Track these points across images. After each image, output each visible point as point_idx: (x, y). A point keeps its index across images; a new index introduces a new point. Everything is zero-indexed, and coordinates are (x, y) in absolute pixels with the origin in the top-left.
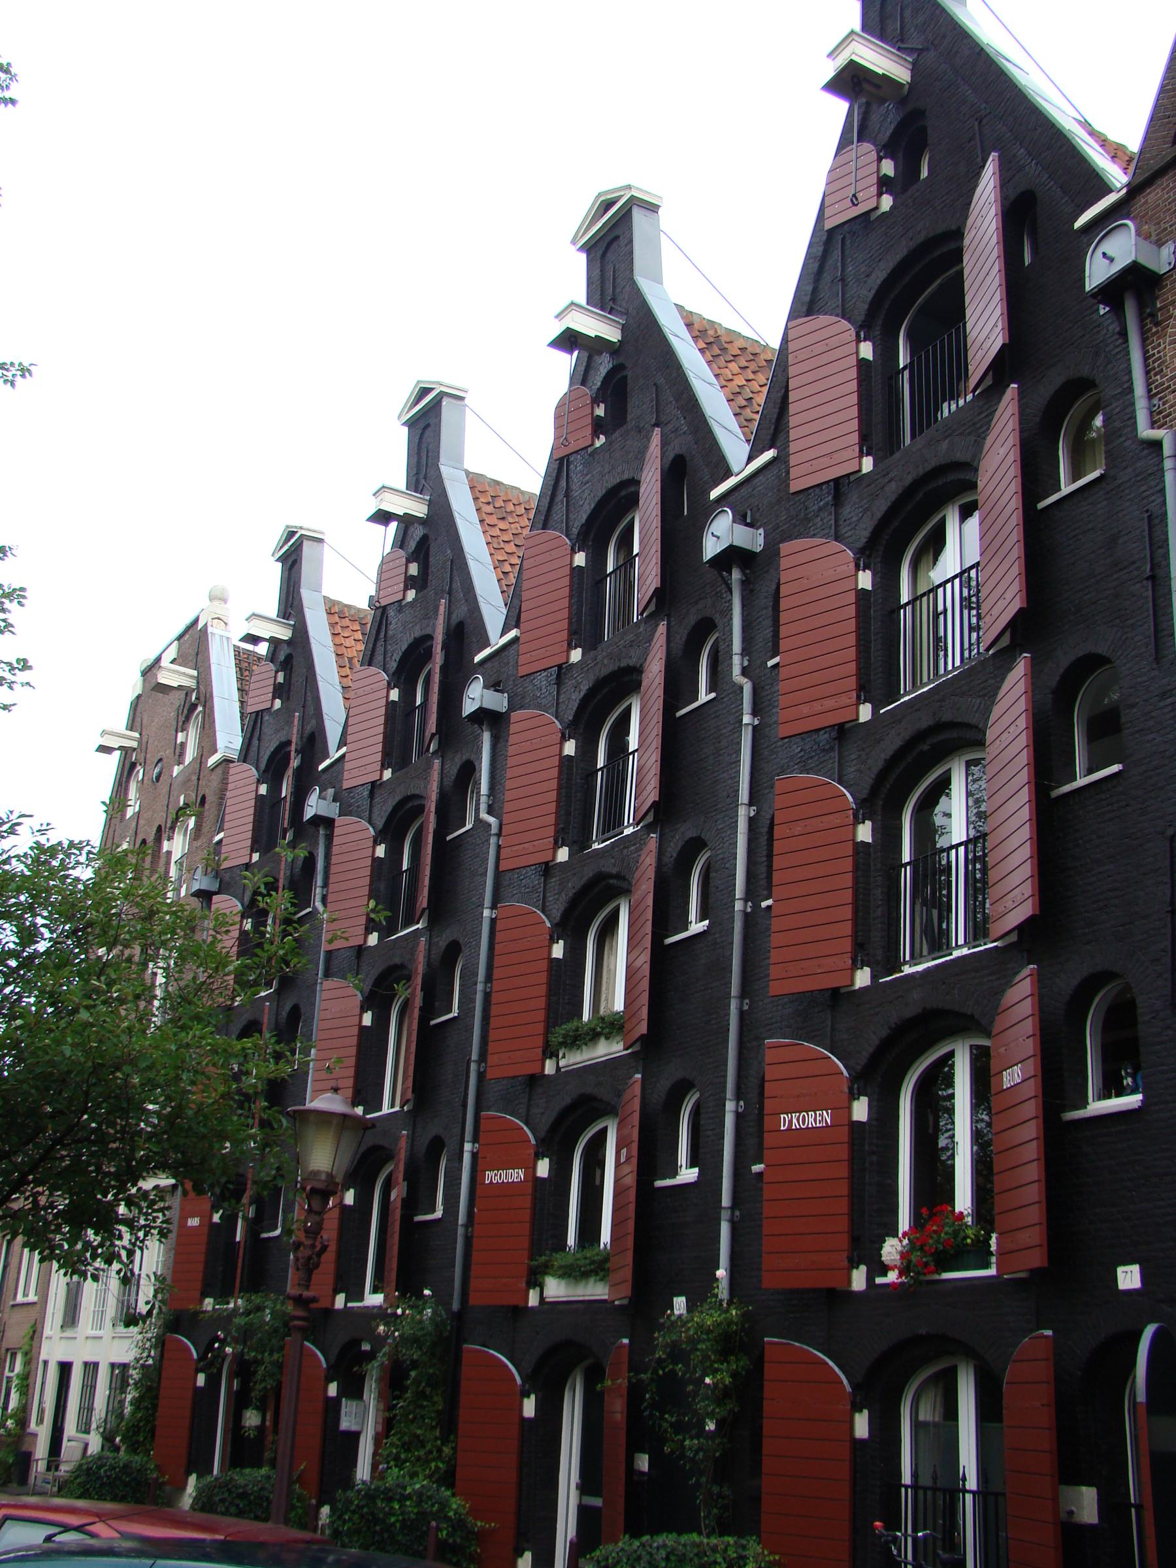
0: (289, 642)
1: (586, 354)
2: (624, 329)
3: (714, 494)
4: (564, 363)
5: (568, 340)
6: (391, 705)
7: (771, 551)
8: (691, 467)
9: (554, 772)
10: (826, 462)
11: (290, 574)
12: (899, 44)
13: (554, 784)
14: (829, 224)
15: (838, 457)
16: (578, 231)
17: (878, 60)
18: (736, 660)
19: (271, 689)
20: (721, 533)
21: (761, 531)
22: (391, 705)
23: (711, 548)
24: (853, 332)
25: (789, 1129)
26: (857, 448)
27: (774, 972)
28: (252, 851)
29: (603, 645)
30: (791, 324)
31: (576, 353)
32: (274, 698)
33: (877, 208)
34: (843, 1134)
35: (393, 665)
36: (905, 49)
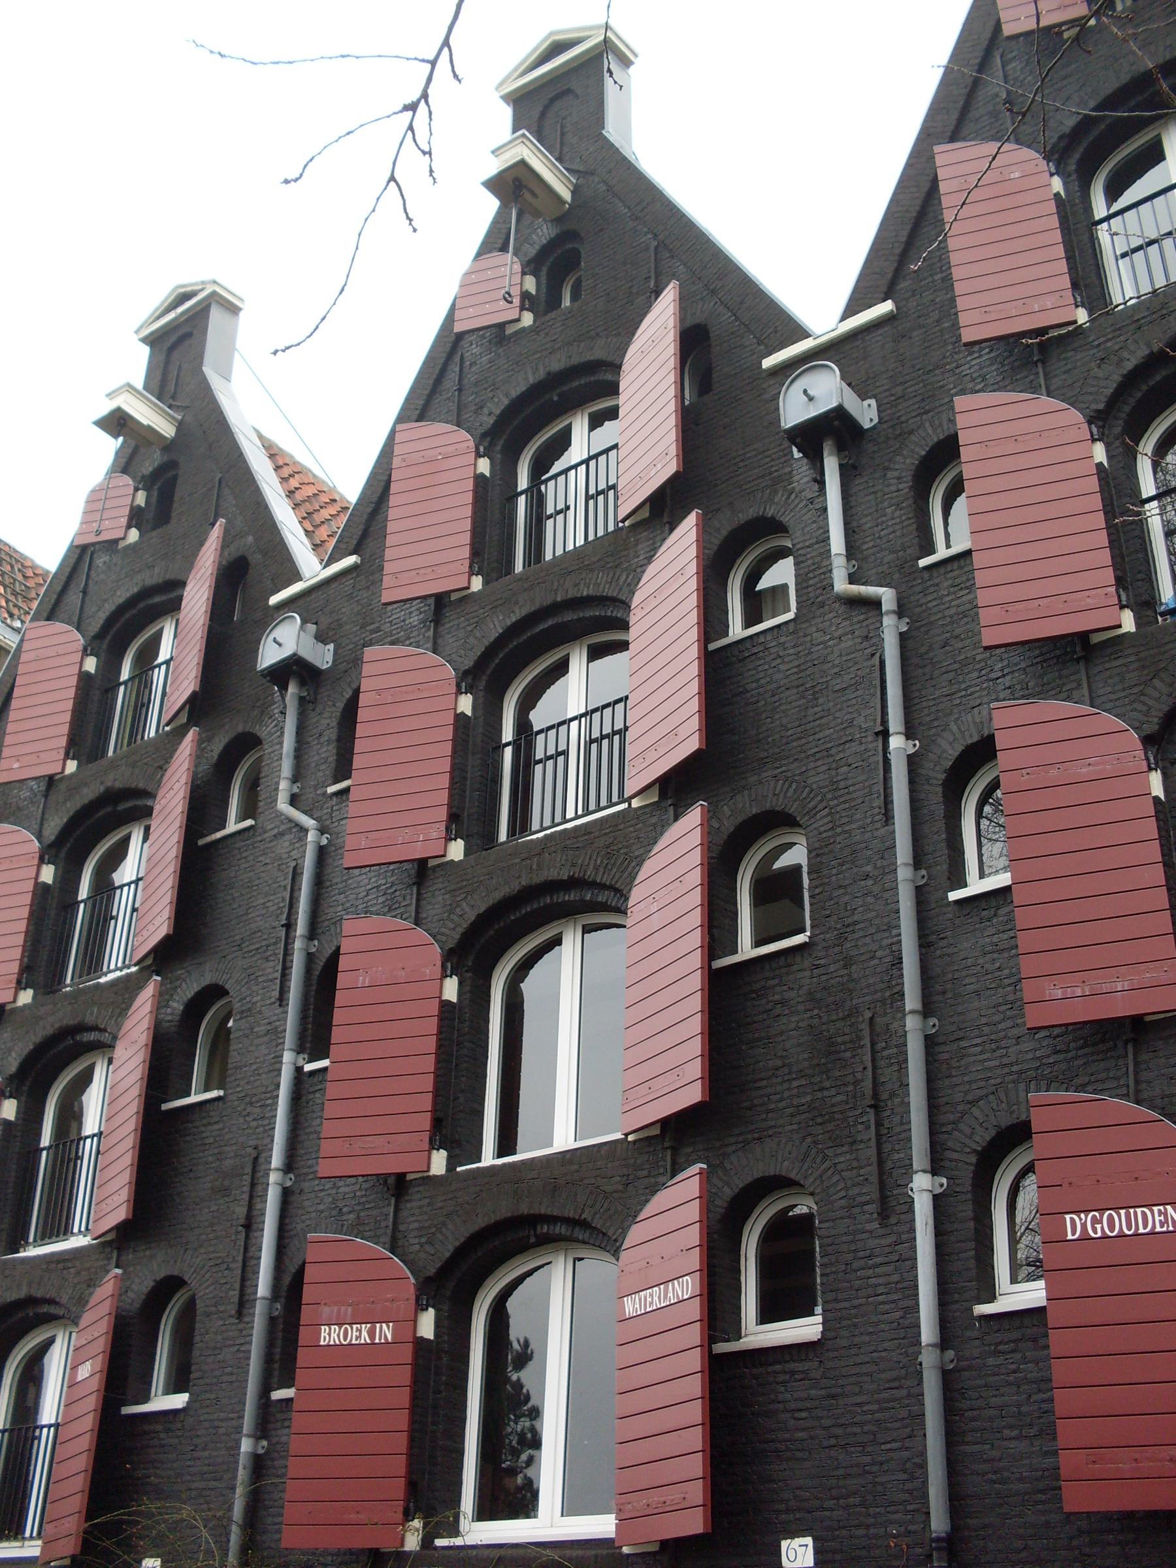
0: (168, 446)
1: (133, 443)
2: (180, 426)
3: (274, 600)
4: (109, 446)
5: (117, 422)
6: (84, 677)
7: (349, 662)
8: (248, 577)
9: (27, 898)
10: (33, 759)
11: (167, 363)
12: (171, 402)
13: (25, 912)
14: (458, 328)
15: (44, 757)
16: (515, 69)
17: (145, 414)
18: (284, 785)
19: (127, 511)
20: (284, 641)
21: (331, 647)
22: (84, 677)
23: (270, 655)
24: (472, 444)
25: (1085, 1238)
26: (62, 751)
27: (326, 1148)
28: (67, 756)
29: (104, 762)
30: (399, 427)
31: (121, 439)
32: (129, 527)
33: (518, 320)
34: (406, 1354)
35: (95, 626)
36: (178, 407)
